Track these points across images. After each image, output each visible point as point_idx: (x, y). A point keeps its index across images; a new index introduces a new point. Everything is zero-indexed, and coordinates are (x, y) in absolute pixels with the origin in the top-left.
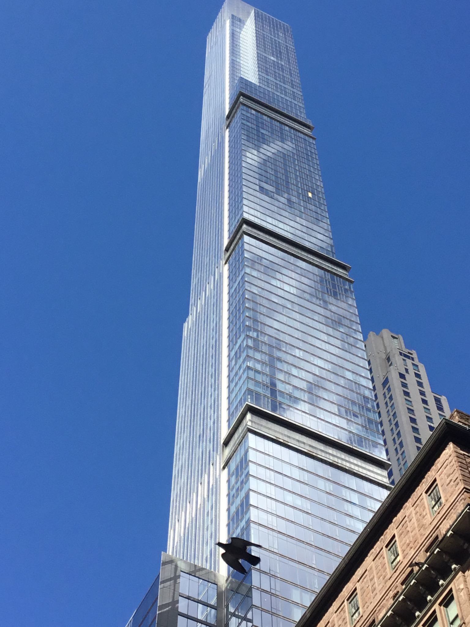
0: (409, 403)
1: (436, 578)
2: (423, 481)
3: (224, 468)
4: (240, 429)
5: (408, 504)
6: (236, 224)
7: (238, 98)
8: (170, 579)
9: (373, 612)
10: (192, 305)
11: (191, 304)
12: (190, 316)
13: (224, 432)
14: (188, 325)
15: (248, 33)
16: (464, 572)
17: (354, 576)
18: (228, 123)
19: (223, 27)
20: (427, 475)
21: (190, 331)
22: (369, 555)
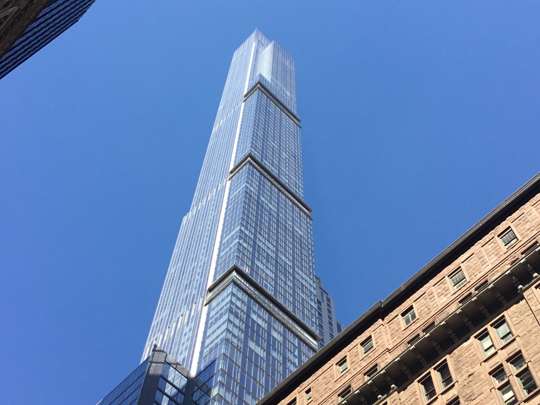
3: (206, 305)
6: (241, 157)
9: (486, 275)
11: (192, 204)
12: (190, 212)
13: (210, 283)
15: (267, 53)
16: (399, 393)
18: (245, 99)
19: (250, 47)
21: (188, 221)
22: (476, 244)
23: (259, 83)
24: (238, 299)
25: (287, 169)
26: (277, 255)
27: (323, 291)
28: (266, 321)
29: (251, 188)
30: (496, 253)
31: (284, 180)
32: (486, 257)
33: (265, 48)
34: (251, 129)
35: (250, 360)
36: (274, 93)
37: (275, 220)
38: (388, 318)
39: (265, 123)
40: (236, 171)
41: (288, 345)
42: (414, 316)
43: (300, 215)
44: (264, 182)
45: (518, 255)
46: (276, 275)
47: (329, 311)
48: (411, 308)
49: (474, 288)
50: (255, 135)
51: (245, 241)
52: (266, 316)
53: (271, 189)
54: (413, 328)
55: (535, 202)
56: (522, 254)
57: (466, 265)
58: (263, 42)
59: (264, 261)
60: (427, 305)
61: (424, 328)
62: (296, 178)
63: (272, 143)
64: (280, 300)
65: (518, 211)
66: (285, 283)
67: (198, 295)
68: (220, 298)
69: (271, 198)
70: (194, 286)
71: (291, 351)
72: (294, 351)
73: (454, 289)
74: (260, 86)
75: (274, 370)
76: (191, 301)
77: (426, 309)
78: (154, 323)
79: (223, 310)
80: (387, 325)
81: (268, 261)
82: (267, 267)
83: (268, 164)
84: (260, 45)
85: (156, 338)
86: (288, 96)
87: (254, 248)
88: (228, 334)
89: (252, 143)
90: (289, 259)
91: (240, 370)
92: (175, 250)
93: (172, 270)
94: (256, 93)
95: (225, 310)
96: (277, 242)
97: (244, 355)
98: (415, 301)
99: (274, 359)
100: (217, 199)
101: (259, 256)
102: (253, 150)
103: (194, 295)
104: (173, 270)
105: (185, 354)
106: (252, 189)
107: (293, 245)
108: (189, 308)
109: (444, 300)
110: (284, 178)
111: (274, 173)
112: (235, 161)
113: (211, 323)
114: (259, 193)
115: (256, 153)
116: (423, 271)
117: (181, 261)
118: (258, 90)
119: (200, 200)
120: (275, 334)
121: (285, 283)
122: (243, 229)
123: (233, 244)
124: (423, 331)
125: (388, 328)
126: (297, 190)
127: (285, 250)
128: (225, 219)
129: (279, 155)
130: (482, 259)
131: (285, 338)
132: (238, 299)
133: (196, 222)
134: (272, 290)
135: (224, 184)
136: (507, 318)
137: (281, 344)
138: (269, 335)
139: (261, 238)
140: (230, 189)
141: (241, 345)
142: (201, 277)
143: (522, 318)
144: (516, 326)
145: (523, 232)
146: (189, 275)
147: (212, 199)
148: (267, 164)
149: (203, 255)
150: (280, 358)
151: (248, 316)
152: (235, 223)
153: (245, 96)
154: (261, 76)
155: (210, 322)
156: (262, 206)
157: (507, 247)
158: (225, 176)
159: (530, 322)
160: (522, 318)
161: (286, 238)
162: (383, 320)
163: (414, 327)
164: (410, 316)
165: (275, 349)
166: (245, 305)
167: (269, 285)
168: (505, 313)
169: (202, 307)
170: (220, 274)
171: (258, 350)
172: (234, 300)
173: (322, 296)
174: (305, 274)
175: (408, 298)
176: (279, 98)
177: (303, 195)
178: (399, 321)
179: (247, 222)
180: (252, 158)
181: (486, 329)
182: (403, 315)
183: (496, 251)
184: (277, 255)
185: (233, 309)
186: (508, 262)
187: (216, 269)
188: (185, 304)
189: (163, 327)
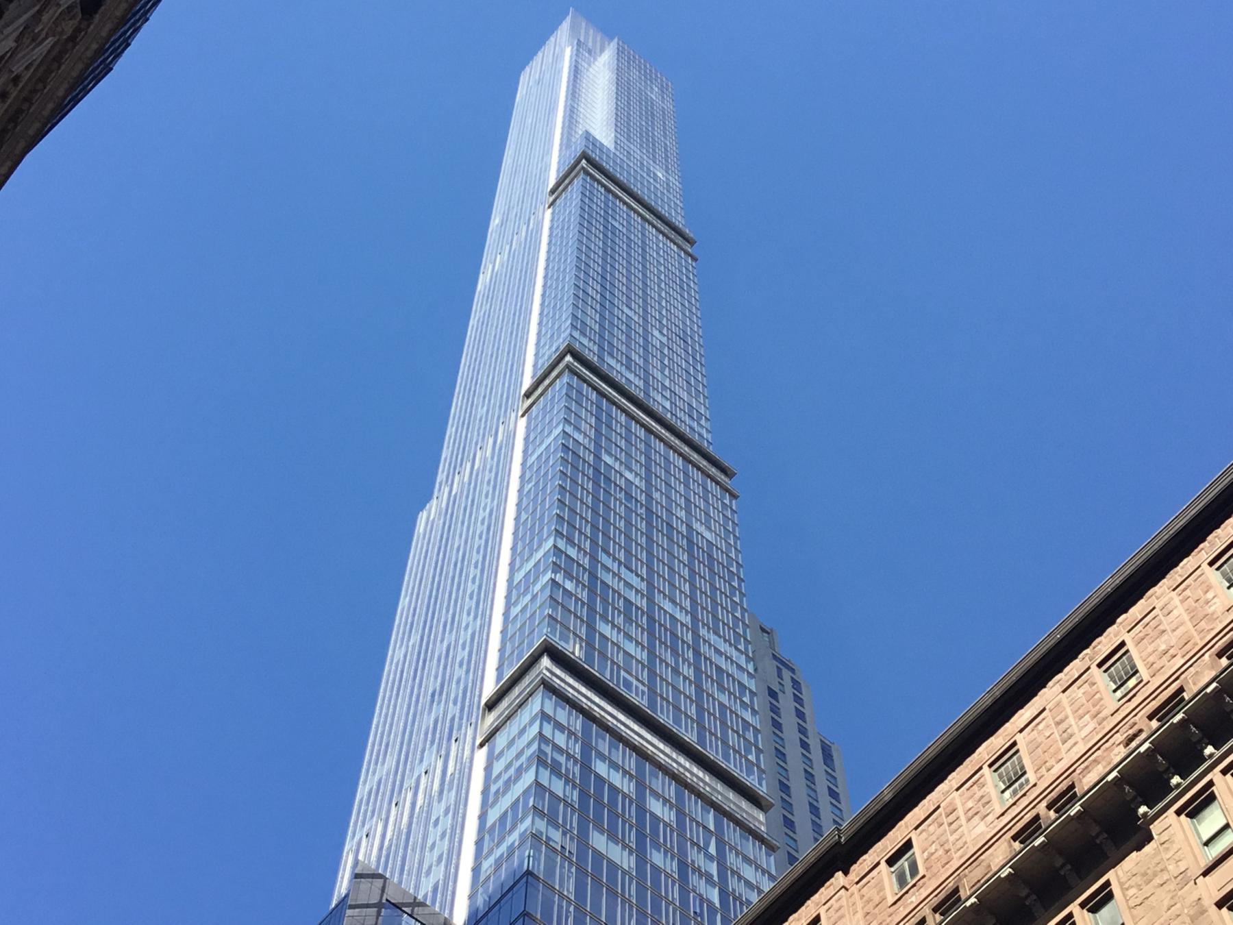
0: (784, 773)
1: (1200, 741)
2: (1201, 546)
3: (481, 745)
4: (526, 680)
5: (1165, 583)
6: (550, 354)
7: (578, 162)
8: (373, 906)
9: (1069, 770)
10: (441, 484)
11: (438, 480)
12: (434, 501)
13: (489, 688)
14: (427, 519)
15: (602, 71)
17: (1007, 725)
18: (551, 199)
19: (558, 58)
20: (1214, 534)
22: (1050, 684)
23: (584, 156)
24: (559, 726)
25: (667, 373)
26: (651, 601)
27: (782, 664)
28: (631, 775)
29: (576, 436)
30: (1094, 711)
31: (660, 403)
32: (1071, 720)
33: (595, 59)
34: (569, 279)
35: (597, 881)
36: (622, 178)
37: (643, 511)
38: (857, 869)
39: (604, 260)
40: (540, 390)
41: (691, 831)
42: (914, 869)
43: (705, 489)
44: (609, 415)
45: (1141, 720)
46: (652, 654)
47: (800, 715)
48: (908, 845)
49: (1044, 804)
50: (580, 295)
51: (568, 575)
52: (631, 763)
53: (628, 430)
54: (913, 899)
55: (1180, 580)
56: (1150, 717)
57: (1029, 738)
58: (590, 45)
59: (620, 620)
60: (943, 839)
61: (936, 901)
62: (689, 394)
63: (626, 310)
64: (665, 718)
65: (1142, 601)
66: (676, 671)
67: (461, 718)
68: (513, 728)
69: (628, 455)
70: (453, 696)
71: (699, 846)
72: (707, 844)
73: (1002, 801)
74: (588, 165)
75: (657, 899)
76: (444, 735)
77: (941, 852)
78: (362, 791)
79: (523, 759)
80: (854, 889)
81: (628, 619)
82: (628, 636)
83: (618, 367)
84: (582, 49)
85: (363, 846)
86: (661, 181)
87: (592, 592)
88: (537, 820)
89: (574, 316)
90: (682, 608)
91: (572, 909)
92: (404, 602)
93: (397, 653)
94: (578, 183)
95: (529, 759)
96: (650, 568)
97: (581, 871)
98: (916, 828)
99: (656, 870)
100: (497, 465)
101: (605, 610)
102: (576, 334)
103: (453, 719)
104: (399, 655)
105: (439, 873)
106: (580, 438)
107: (692, 571)
108: (443, 753)
109: (981, 830)
110: (659, 398)
111: (632, 389)
112: (535, 366)
113: (497, 791)
114: (598, 445)
115: (585, 341)
116: (932, 753)
117: (417, 631)
118: (582, 175)
119: (455, 469)
120: (656, 807)
121: (676, 671)
122: (561, 544)
123: (538, 587)
124: (935, 910)
125: (857, 896)
126: (695, 425)
127: (672, 585)
128: (517, 519)
129: (645, 339)
130: (1063, 726)
131: (681, 814)
132: (559, 726)
133: (448, 528)
134: (643, 692)
135: (512, 426)
136: (1115, 888)
137: (672, 831)
138: (642, 810)
139: (608, 562)
140: (526, 439)
141: (571, 846)
142: (468, 671)
143: (1148, 890)
144: (1134, 912)
145: (1151, 659)
146: (438, 666)
147: (485, 467)
148: (614, 366)
149: (469, 614)
150: (672, 867)
151: (586, 767)
152: (541, 530)
153: (552, 192)
154: (588, 136)
155: (493, 788)
156: (608, 479)
157: (1119, 694)
158: (513, 404)
159: (1166, 903)
160: (1148, 890)
161: (670, 554)
162: (846, 873)
163: (913, 899)
164: (906, 864)
165: (656, 846)
166: (576, 741)
167: (635, 682)
168: (1110, 875)
169: (473, 751)
170: (511, 665)
171: (616, 853)
172: (548, 730)
173: (780, 676)
174: (725, 641)
175: (901, 819)
176: (637, 189)
177: (709, 437)
178: (882, 880)
179: (571, 525)
180: (577, 356)
181: (1070, 916)
182: (891, 862)
183: (1094, 706)
184: (651, 601)
185: (546, 754)
186: (1119, 737)
187: (502, 650)
188: (432, 742)
189: (382, 800)
